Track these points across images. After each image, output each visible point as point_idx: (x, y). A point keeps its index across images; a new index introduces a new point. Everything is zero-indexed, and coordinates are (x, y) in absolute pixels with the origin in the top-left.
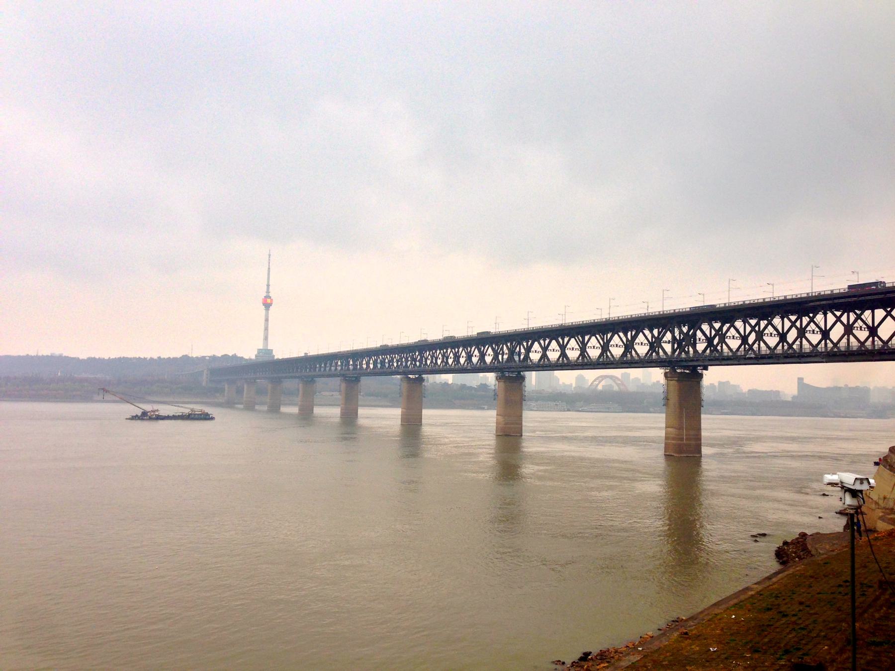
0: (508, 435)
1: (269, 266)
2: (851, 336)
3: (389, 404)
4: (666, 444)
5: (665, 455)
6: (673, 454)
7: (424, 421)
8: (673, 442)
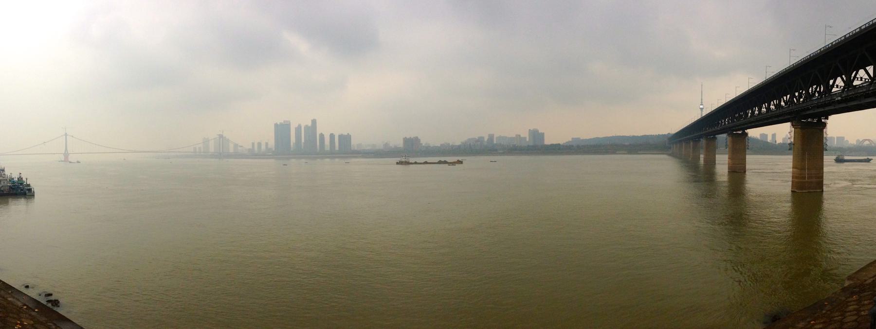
4: (793, 182)
5: (792, 191)
6: (796, 190)
8: (796, 180)
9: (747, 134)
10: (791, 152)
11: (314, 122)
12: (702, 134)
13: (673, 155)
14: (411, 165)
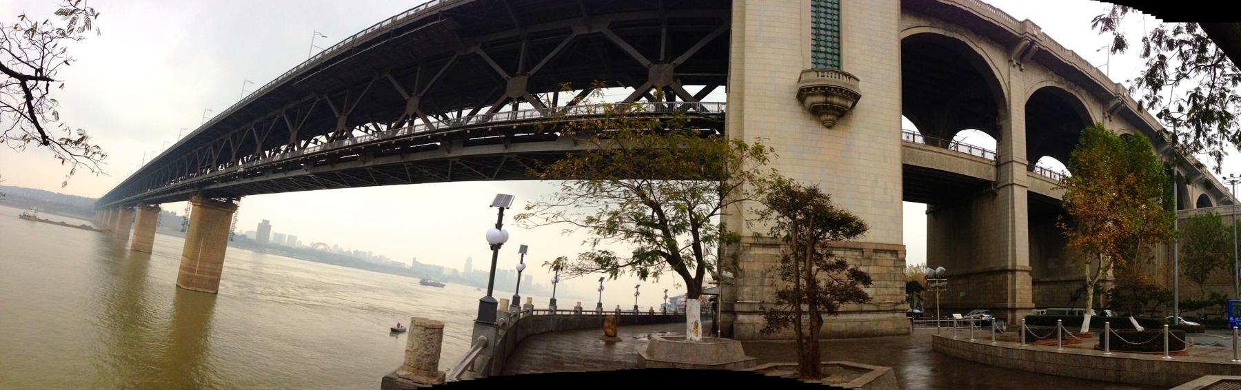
4: (179, 273)
5: (177, 285)
8: (183, 272)
9: (159, 209)
10: (184, 234)
11: (652, 308)
14: (38, 224)
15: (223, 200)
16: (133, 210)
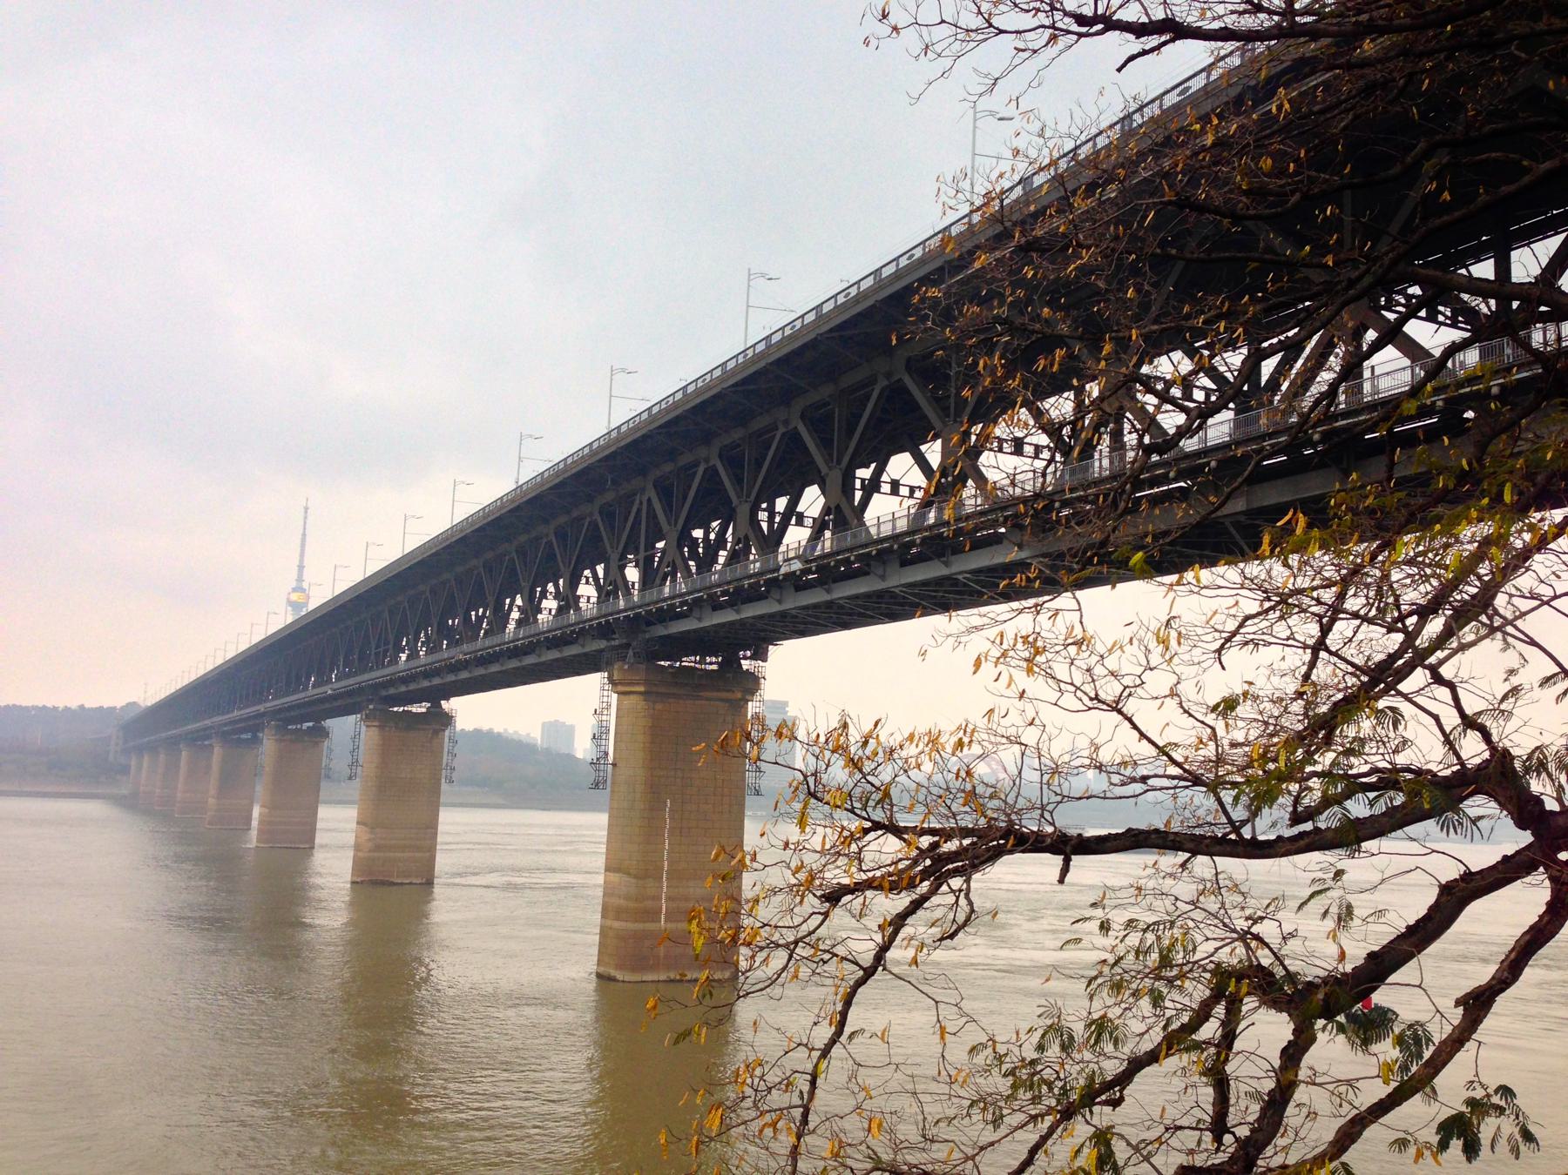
0: (383, 883)
1: (305, 529)
2: (1025, 441)
3: (501, 801)
4: (604, 933)
5: (599, 976)
6: (613, 973)
7: (320, 839)
8: (617, 924)
9: (447, 719)
10: (604, 795)
12: (263, 715)
13: (131, 803)
15: (419, 708)
16: (256, 741)
